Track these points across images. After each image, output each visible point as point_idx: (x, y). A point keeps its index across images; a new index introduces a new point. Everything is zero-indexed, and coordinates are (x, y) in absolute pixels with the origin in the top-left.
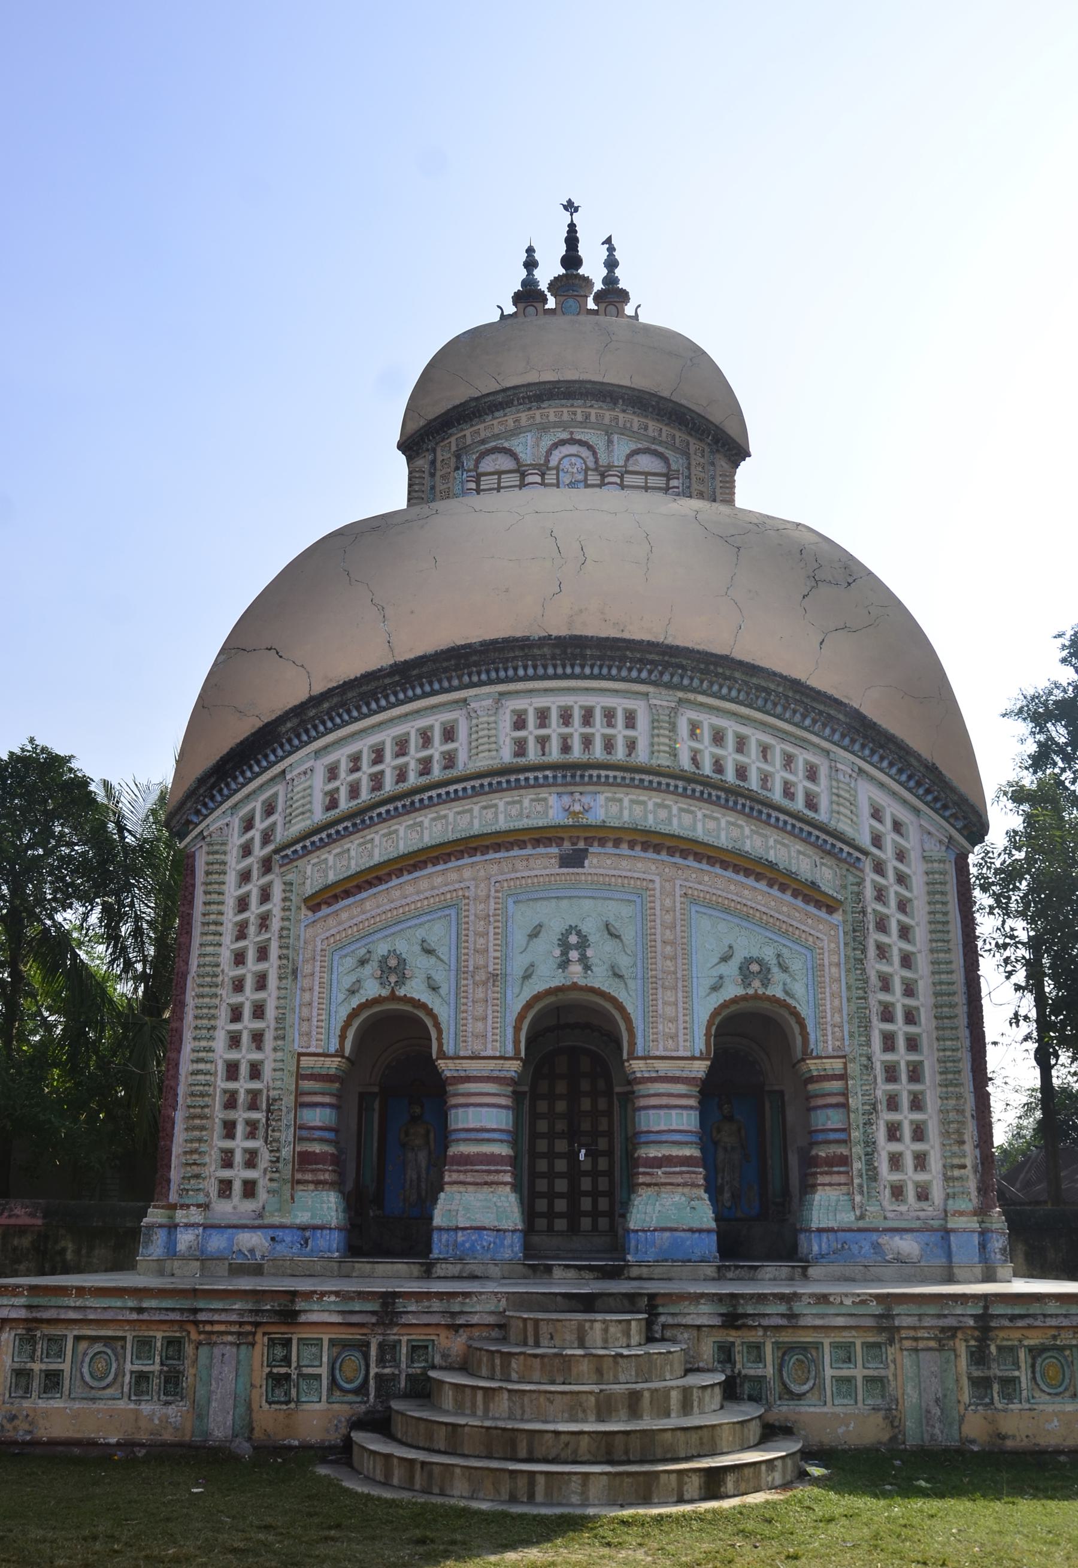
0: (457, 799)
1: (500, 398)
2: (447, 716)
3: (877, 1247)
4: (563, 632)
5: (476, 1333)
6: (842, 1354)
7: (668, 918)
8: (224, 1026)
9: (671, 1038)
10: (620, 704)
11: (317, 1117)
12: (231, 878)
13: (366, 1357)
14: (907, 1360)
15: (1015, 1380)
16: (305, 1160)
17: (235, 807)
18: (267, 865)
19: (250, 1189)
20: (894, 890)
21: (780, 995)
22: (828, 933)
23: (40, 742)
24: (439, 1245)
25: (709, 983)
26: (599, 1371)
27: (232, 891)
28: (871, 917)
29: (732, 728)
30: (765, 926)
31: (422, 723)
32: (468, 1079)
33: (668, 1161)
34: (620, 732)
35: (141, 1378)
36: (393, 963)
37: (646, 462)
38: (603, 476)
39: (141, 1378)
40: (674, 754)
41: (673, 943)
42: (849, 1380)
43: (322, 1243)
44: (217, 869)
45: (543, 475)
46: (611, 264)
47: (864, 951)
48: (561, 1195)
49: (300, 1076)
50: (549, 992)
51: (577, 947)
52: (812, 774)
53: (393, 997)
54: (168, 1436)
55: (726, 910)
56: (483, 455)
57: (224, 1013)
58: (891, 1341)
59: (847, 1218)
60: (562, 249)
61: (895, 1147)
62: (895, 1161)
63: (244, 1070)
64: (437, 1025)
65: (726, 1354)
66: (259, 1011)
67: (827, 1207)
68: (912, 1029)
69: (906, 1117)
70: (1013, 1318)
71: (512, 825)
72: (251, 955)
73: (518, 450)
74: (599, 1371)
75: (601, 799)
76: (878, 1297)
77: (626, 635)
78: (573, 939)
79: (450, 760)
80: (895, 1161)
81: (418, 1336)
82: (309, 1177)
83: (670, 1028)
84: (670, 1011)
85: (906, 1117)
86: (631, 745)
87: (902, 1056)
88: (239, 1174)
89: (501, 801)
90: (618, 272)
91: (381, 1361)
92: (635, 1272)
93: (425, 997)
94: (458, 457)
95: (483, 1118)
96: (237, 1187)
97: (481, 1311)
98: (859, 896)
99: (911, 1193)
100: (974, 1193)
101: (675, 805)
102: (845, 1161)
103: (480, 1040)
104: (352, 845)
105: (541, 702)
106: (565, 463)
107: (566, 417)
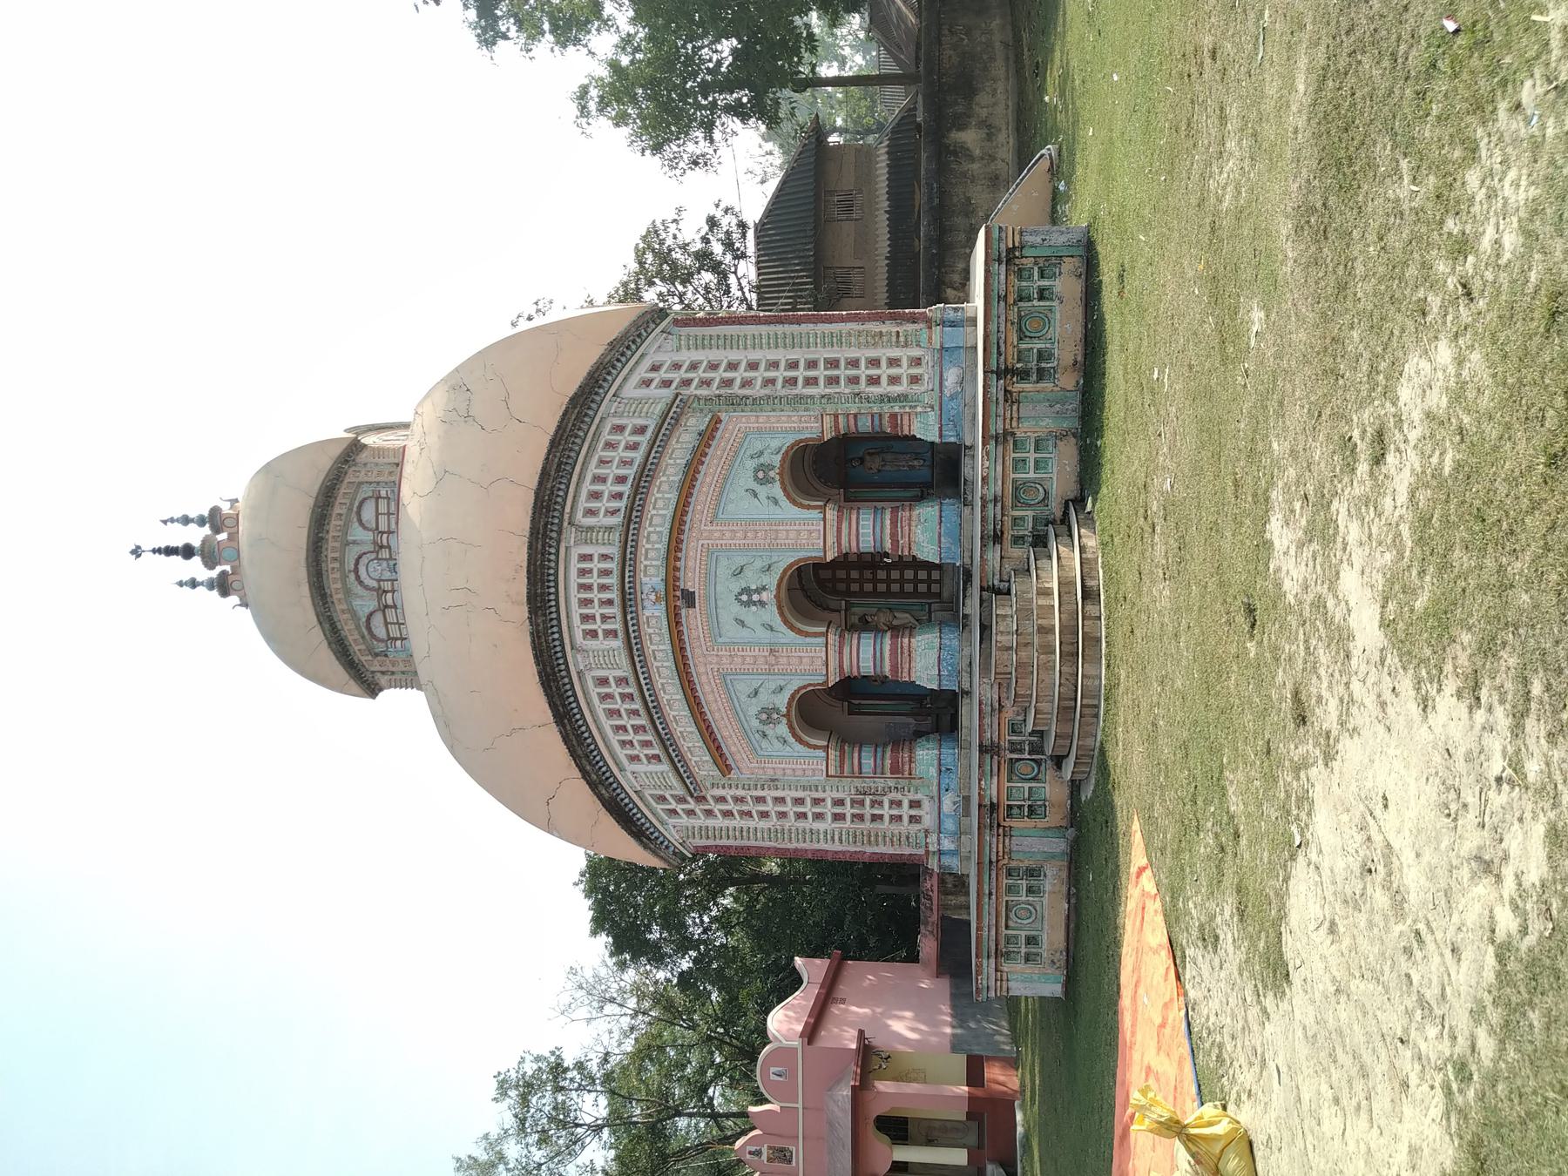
0: (650, 677)
1: (327, 626)
2: (590, 683)
3: (952, 398)
4: (526, 609)
5: (1004, 695)
6: (1020, 465)
7: (728, 534)
8: (809, 824)
9: (812, 531)
10: (575, 565)
11: (868, 762)
12: (710, 822)
13: (1018, 760)
14: (1025, 425)
15: (1040, 352)
16: (896, 769)
17: (662, 823)
18: (701, 799)
19: (915, 804)
20: (701, 373)
21: (779, 457)
22: (735, 424)
23: (577, 877)
24: (950, 685)
25: (772, 506)
26: (1026, 645)
27: (719, 822)
28: (722, 391)
29: (587, 486)
30: (731, 466)
31: (596, 700)
32: (841, 666)
33: (894, 535)
34: (596, 565)
35: (1030, 890)
36: (764, 716)
37: (368, 513)
38: (382, 547)
39: (1030, 890)
40: (610, 529)
41: (746, 532)
42: (1036, 462)
43: (949, 760)
44: (705, 831)
45: (386, 592)
46: (186, 520)
47: (747, 398)
48: (916, 575)
49: (841, 776)
50: (782, 614)
51: (750, 596)
52: (620, 429)
53: (787, 715)
54: (1064, 874)
55: (721, 494)
56: (373, 636)
57: (801, 824)
58: (1013, 434)
59: (932, 417)
60: (177, 560)
61: (884, 380)
62: (894, 380)
63: (838, 810)
64: (804, 687)
65: (1017, 540)
66: (799, 801)
67: (926, 428)
68: (802, 364)
69: (863, 372)
70: (999, 354)
71: (667, 641)
72: (762, 808)
73: (367, 611)
74: (1026, 645)
75: (645, 580)
76: (984, 444)
77: (525, 564)
78: (744, 598)
79: (622, 681)
80: (894, 380)
81: (1005, 729)
82: (907, 767)
83: (804, 535)
84: (792, 535)
85: (863, 372)
86: (604, 557)
87: (821, 373)
88: (905, 811)
89: (650, 648)
90: (192, 515)
91: (1021, 751)
92: (967, 561)
93: (787, 695)
94: (377, 655)
95: (867, 655)
96: (913, 812)
97: (991, 694)
98: (708, 400)
99: (915, 371)
100: (916, 326)
101: (647, 529)
102: (893, 416)
103: (814, 657)
104: (685, 745)
105: (576, 620)
106: (376, 575)
107: (337, 575)
